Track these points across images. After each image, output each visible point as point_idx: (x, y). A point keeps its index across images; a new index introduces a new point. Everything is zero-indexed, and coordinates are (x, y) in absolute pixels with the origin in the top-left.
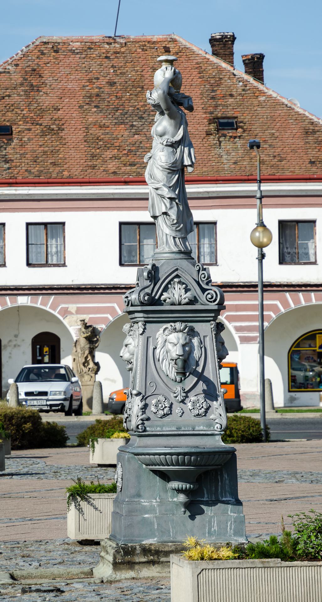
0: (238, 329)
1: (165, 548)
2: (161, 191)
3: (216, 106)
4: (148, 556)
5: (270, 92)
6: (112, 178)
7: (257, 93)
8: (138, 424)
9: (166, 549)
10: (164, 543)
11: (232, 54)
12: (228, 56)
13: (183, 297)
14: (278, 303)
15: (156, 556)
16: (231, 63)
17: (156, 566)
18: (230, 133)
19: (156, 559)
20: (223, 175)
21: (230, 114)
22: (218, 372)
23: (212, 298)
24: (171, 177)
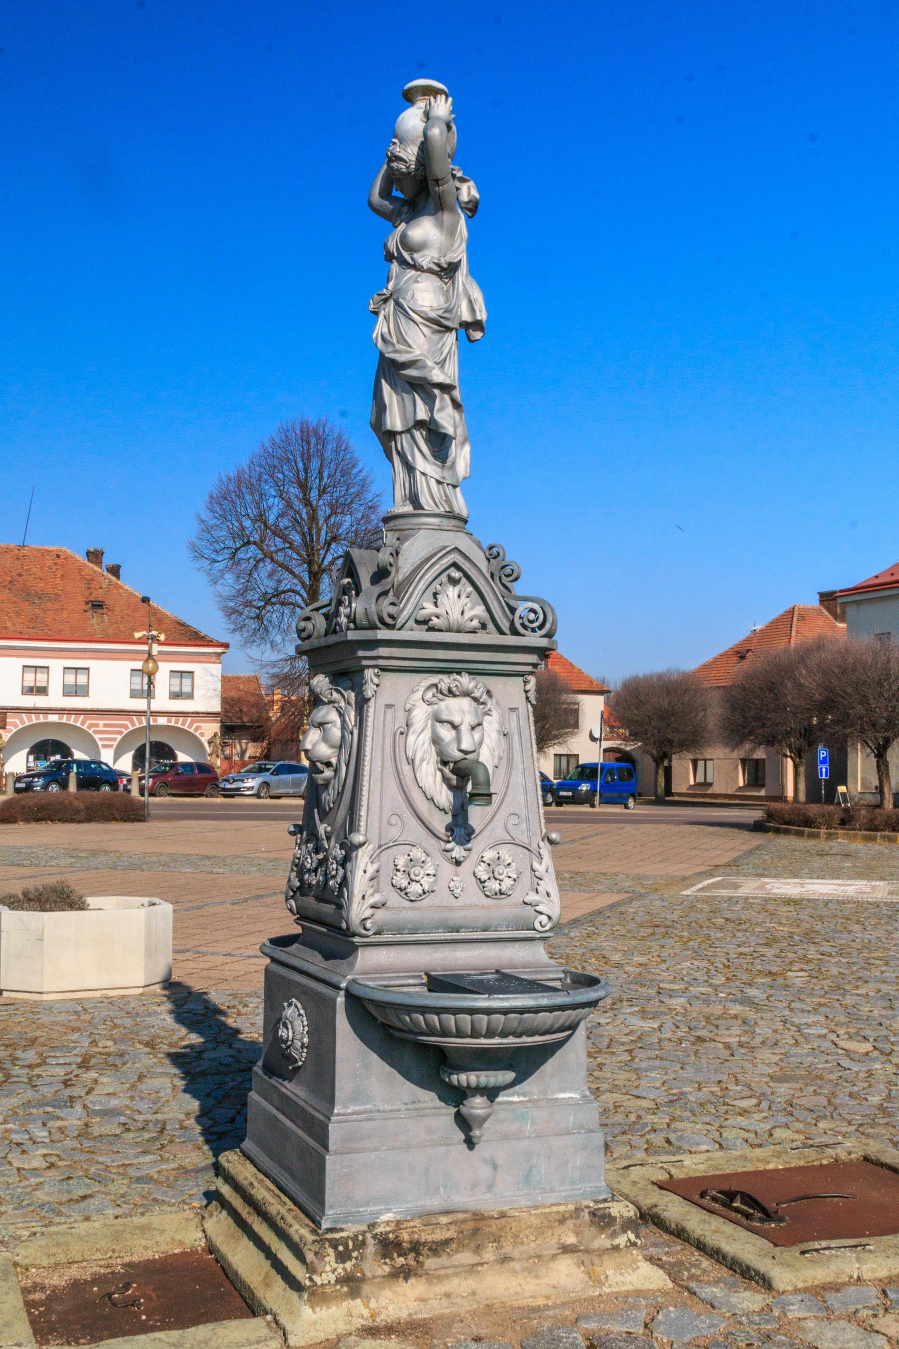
0: (101, 739)
1: (433, 1233)
2: (418, 368)
3: (90, 594)
4: (392, 1259)
5: (126, 587)
6: (19, 636)
7: (117, 587)
8: (364, 916)
9: (439, 1235)
10: (428, 1217)
11: (101, 562)
12: (99, 563)
13: (467, 615)
14: (128, 723)
15: (412, 1256)
16: (101, 567)
17: (412, 1280)
18: (100, 611)
19: (412, 1263)
20: (96, 639)
21: (100, 599)
22: (676, 798)
23: (531, 622)
24: (438, 343)
